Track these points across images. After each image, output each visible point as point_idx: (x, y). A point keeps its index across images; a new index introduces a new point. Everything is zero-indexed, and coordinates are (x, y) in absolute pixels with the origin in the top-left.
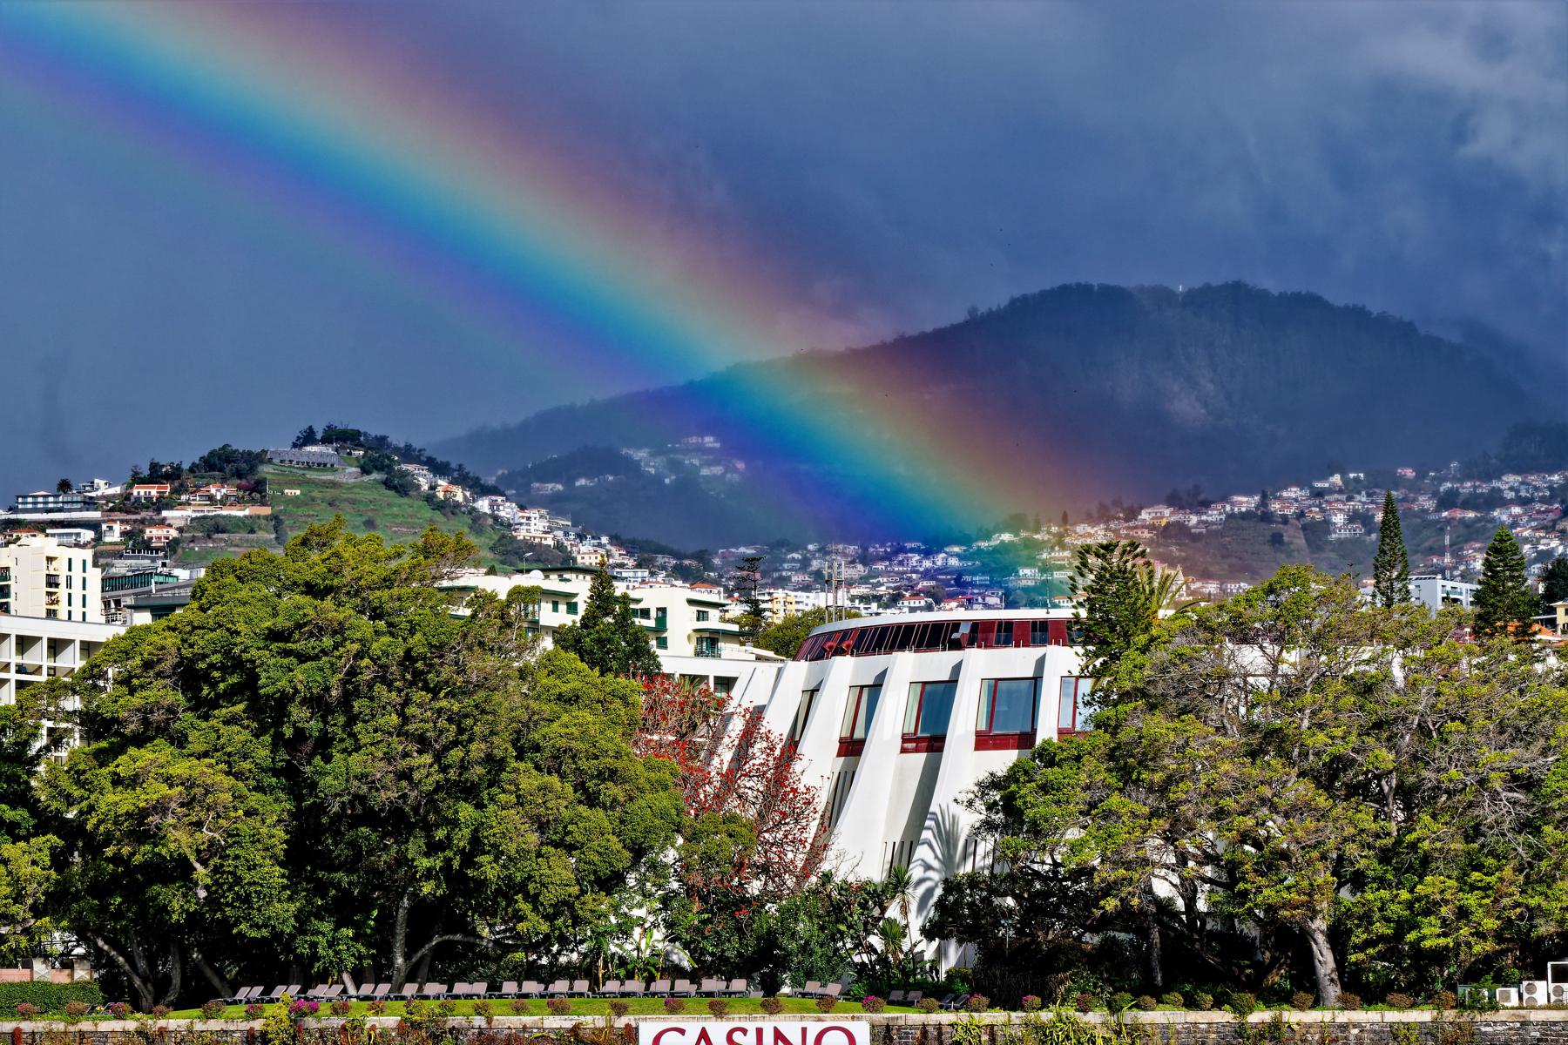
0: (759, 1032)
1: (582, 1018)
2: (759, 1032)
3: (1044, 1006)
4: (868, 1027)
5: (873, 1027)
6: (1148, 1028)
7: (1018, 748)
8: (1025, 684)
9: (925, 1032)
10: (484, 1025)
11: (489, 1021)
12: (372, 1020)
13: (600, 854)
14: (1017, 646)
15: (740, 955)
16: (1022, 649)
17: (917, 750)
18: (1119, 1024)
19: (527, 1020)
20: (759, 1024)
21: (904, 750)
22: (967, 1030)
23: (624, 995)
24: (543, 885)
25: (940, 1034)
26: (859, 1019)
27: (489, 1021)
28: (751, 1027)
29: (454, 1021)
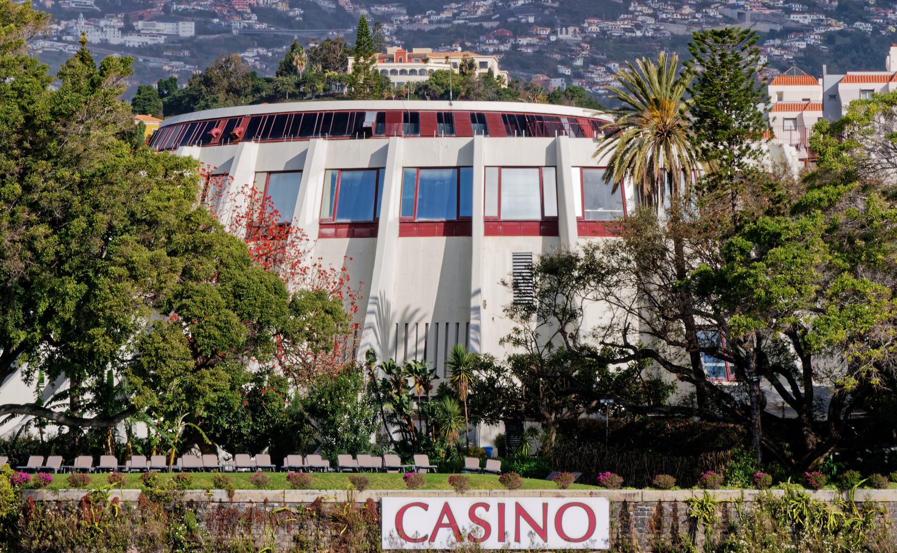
0: (501, 507)
1: (323, 493)
2: (501, 507)
3: (775, 483)
4: (607, 504)
5: (611, 503)
6: (881, 506)
7: (444, 235)
8: (447, 174)
9: (660, 509)
10: (225, 498)
11: (230, 494)
12: (114, 493)
13: (219, 328)
14: (519, 135)
15: (254, 432)
16: (292, 143)
17: (336, 235)
18: (849, 502)
19: (269, 494)
20: (501, 500)
21: (322, 236)
22: (702, 506)
23: (305, 470)
24: (160, 358)
25: (675, 510)
26: (597, 495)
27: (230, 494)
28: (493, 502)
29: (190, 495)
